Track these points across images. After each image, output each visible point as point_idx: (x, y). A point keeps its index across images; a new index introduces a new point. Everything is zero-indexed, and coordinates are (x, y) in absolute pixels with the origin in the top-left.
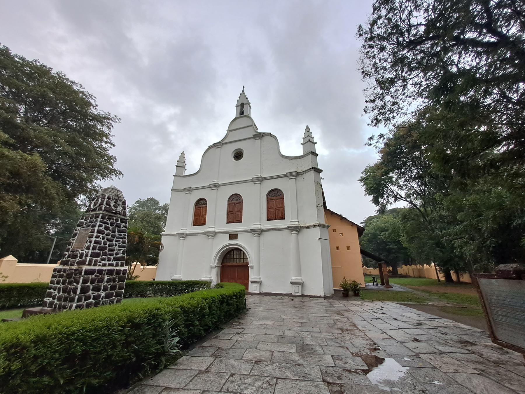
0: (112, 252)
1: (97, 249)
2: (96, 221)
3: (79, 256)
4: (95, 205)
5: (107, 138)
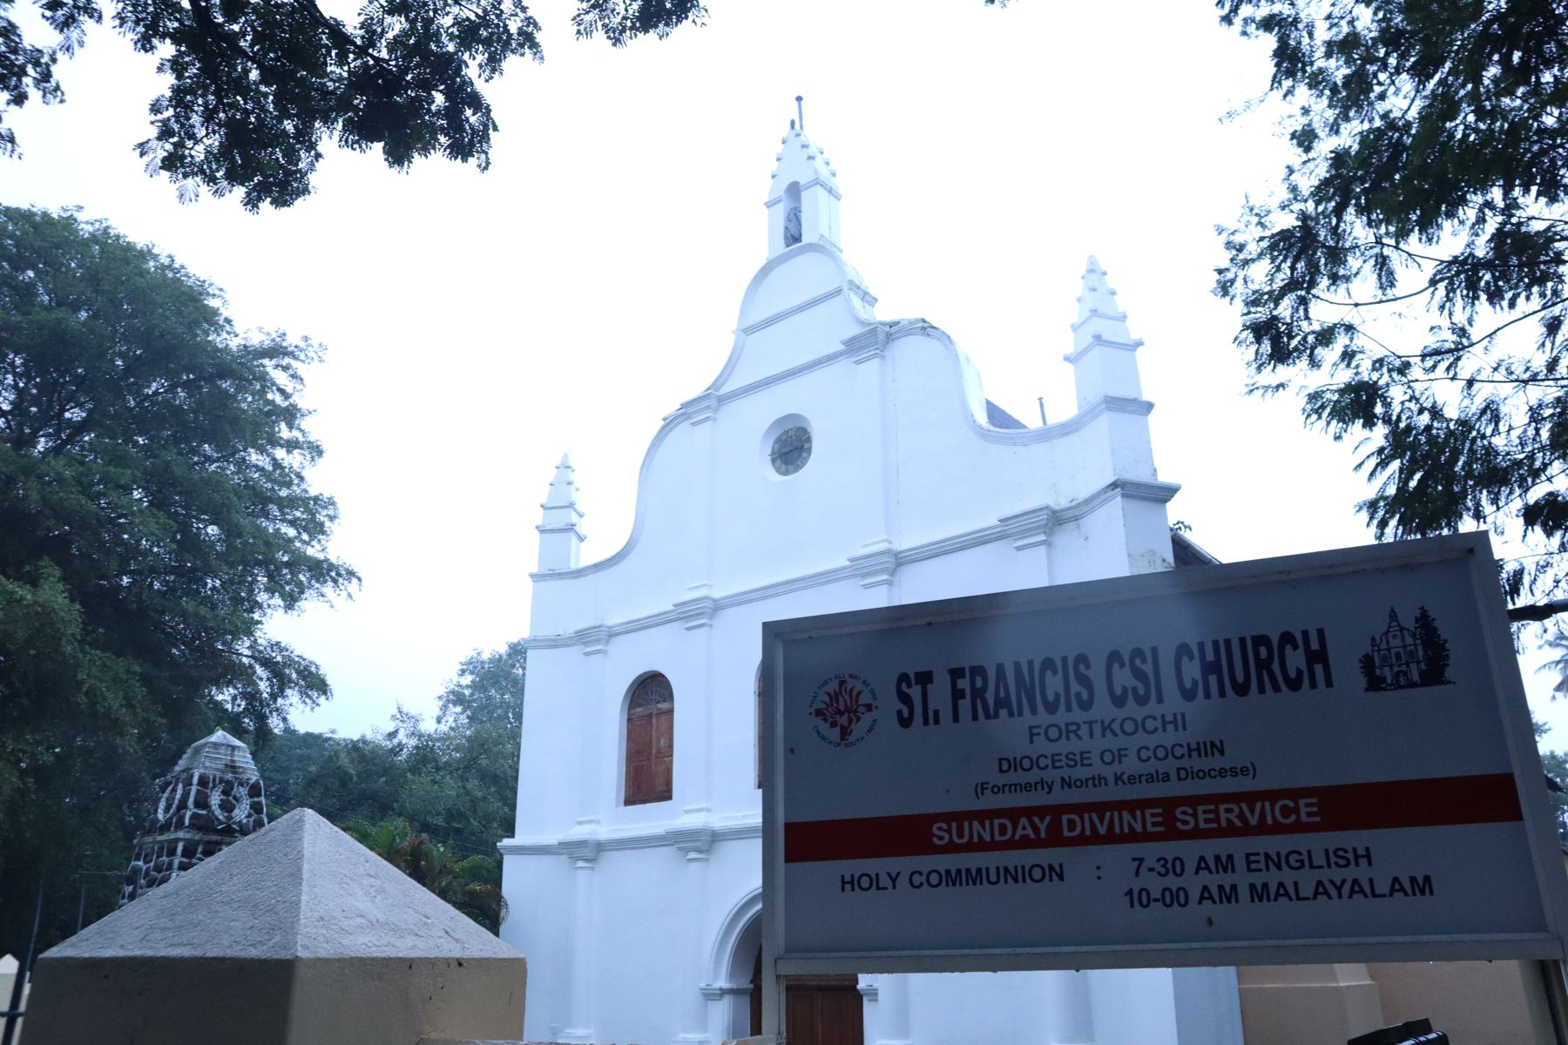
5: (291, 427)
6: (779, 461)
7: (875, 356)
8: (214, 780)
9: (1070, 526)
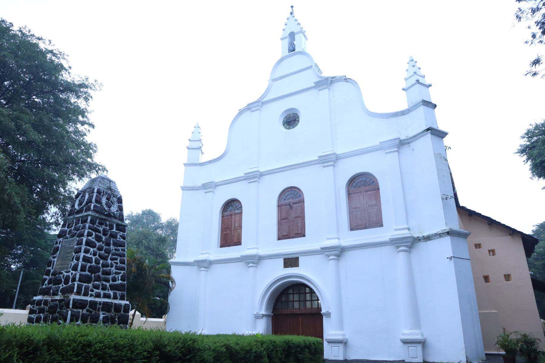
0: (107, 276)
1: (87, 269)
2: (84, 227)
3: (63, 280)
4: (80, 204)
5: (83, 117)
6: (286, 125)
7: (327, 88)
8: (103, 192)
9: (407, 145)
